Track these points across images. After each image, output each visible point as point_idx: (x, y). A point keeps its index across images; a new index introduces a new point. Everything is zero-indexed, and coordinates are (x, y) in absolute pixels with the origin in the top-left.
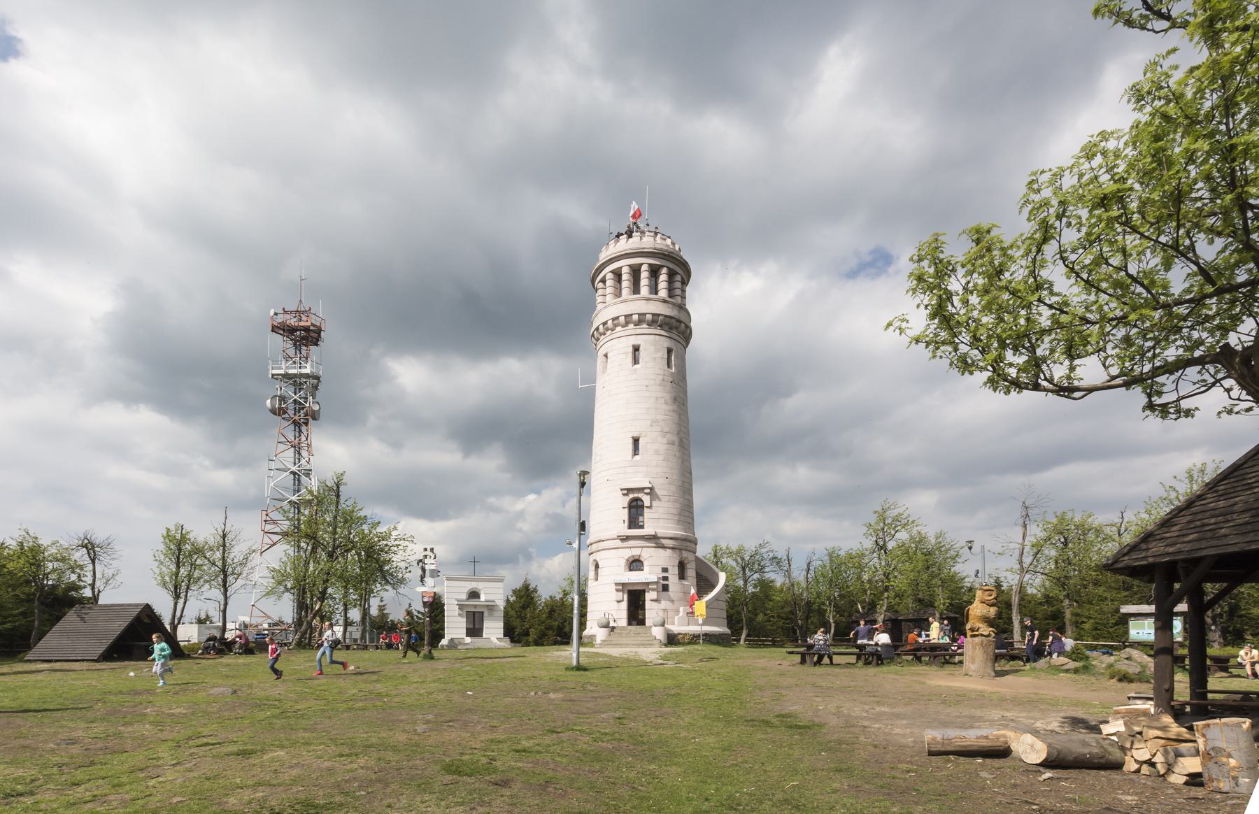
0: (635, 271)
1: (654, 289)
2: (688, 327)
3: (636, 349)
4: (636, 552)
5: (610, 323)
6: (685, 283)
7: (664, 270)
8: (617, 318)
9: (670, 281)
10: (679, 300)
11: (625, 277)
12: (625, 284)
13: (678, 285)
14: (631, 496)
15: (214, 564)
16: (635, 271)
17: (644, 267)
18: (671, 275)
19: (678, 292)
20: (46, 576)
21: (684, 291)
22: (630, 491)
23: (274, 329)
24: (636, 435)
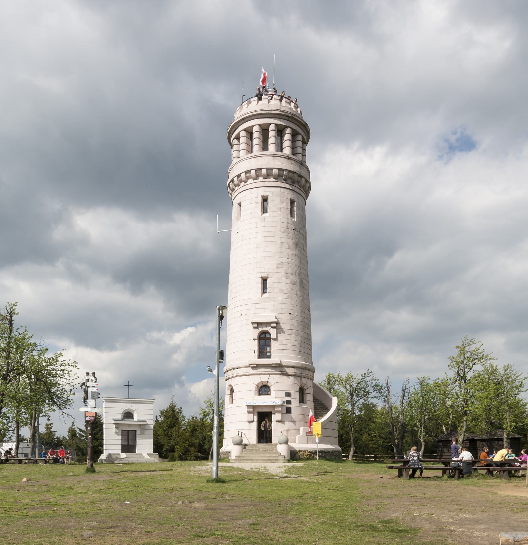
3: (265, 200)
5: (236, 179)
6: (305, 142)
11: (256, 135)
12: (256, 141)
13: (299, 144)
14: (261, 329)
17: (272, 127)
18: (294, 134)
19: (300, 150)
21: (304, 150)
24: (264, 275)
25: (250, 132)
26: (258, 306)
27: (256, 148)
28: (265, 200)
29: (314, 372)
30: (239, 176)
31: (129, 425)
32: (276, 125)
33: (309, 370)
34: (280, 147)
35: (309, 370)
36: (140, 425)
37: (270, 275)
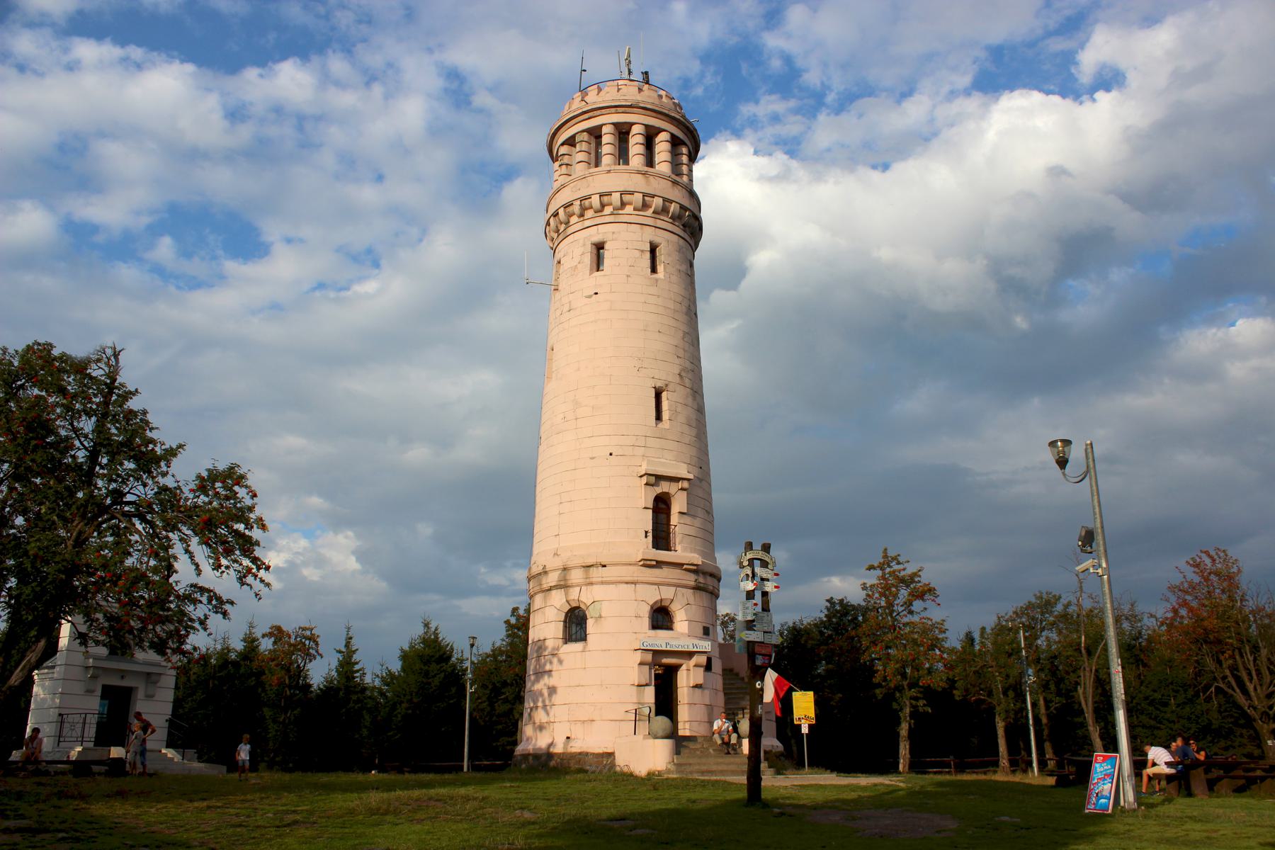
0: (622, 132)
1: (650, 162)
2: (697, 218)
3: (599, 247)
4: (667, 593)
5: (561, 212)
6: (693, 158)
7: (663, 136)
8: (609, 194)
9: (675, 153)
10: (685, 179)
11: (605, 139)
12: (606, 149)
13: (685, 159)
14: (659, 490)
15: (457, 88)
16: (622, 132)
17: (636, 129)
18: (675, 142)
19: (685, 168)
20: (11, 363)
21: (691, 171)
22: (659, 478)
23: (181, 446)
24: (659, 384)
25: (596, 133)
26: (651, 442)
27: (606, 160)
28: (653, 250)
29: (719, 580)
30: (567, 206)
31: (123, 674)
32: (646, 126)
33: (712, 575)
34: (650, 162)
35: (712, 575)
36: (149, 674)
37: (670, 388)
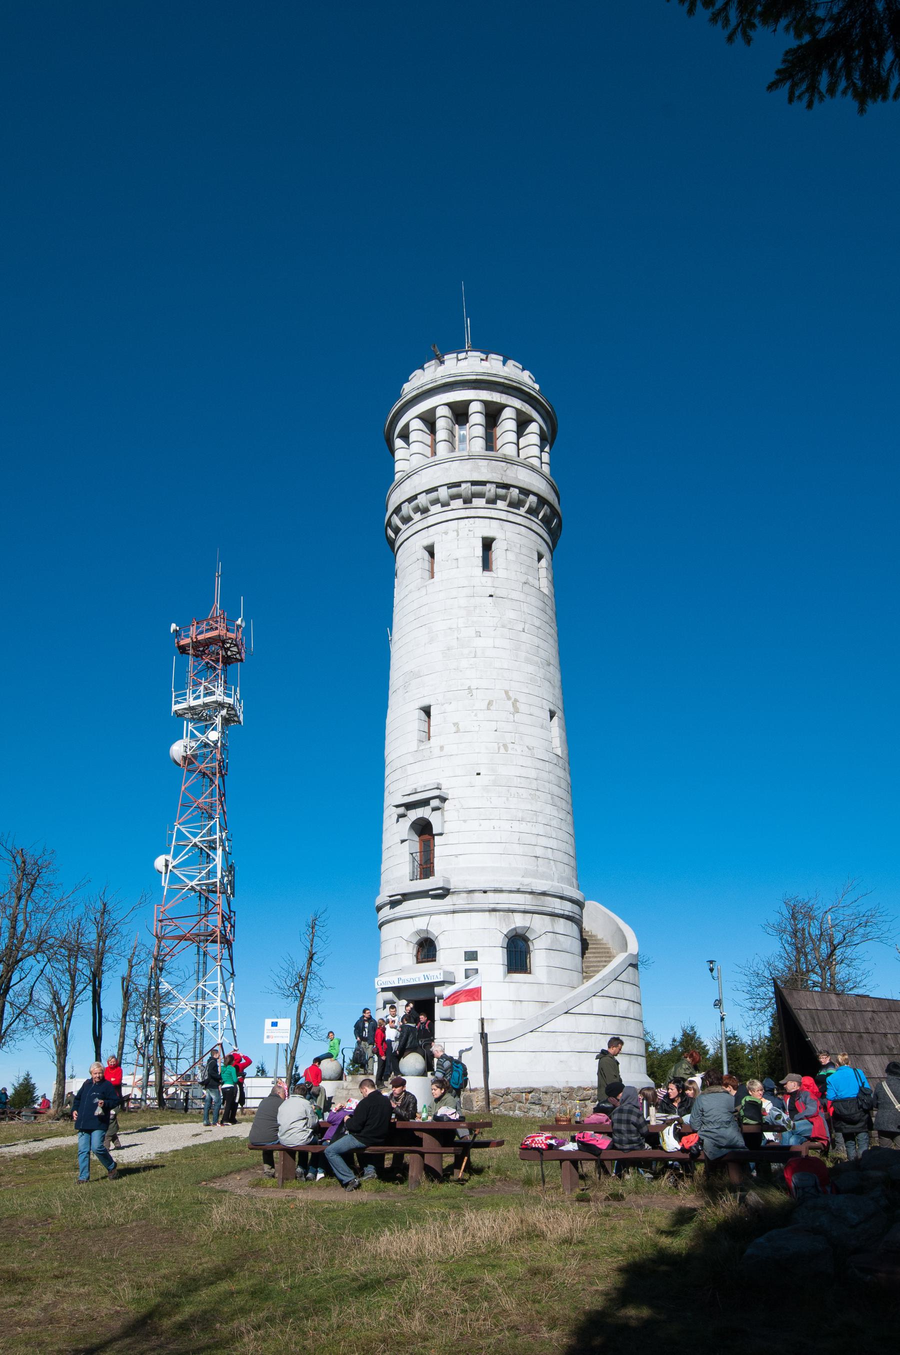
3: (487, 544)
